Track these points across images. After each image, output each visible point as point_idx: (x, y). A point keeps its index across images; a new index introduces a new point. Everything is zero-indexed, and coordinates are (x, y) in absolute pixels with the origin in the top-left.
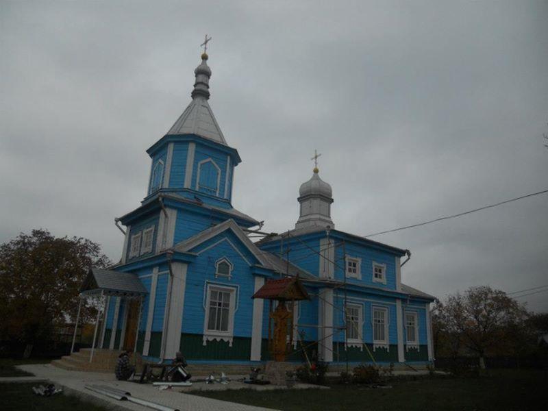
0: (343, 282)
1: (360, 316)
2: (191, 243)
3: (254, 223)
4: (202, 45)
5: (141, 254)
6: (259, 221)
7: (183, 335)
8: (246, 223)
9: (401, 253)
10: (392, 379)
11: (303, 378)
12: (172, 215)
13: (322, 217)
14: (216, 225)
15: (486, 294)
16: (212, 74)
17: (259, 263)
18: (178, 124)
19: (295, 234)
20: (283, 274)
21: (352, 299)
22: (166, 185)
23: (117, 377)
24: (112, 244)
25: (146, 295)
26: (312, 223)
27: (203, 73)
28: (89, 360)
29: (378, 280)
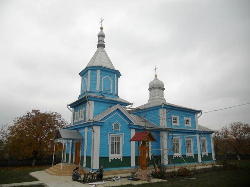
0: (171, 128)
1: (180, 143)
2: (102, 116)
3: (129, 104)
4: (100, 23)
5: (80, 121)
6: (131, 103)
7: (100, 158)
8: (125, 104)
9: (197, 112)
10: (196, 172)
11: (155, 175)
12: (92, 103)
13: (159, 97)
14: (111, 107)
15: (240, 126)
16: (106, 36)
17: (132, 123)
18: (91, 61)
19: (148, 106)
20: (143, 127)
21: (175, 135)
22: (88, 90)
23: (73, 180)
24: (67, 117)
25: (83, 140)
26: (155, 100)
27: (101, 36)
28: (60, 170)
29: (187, 125)
